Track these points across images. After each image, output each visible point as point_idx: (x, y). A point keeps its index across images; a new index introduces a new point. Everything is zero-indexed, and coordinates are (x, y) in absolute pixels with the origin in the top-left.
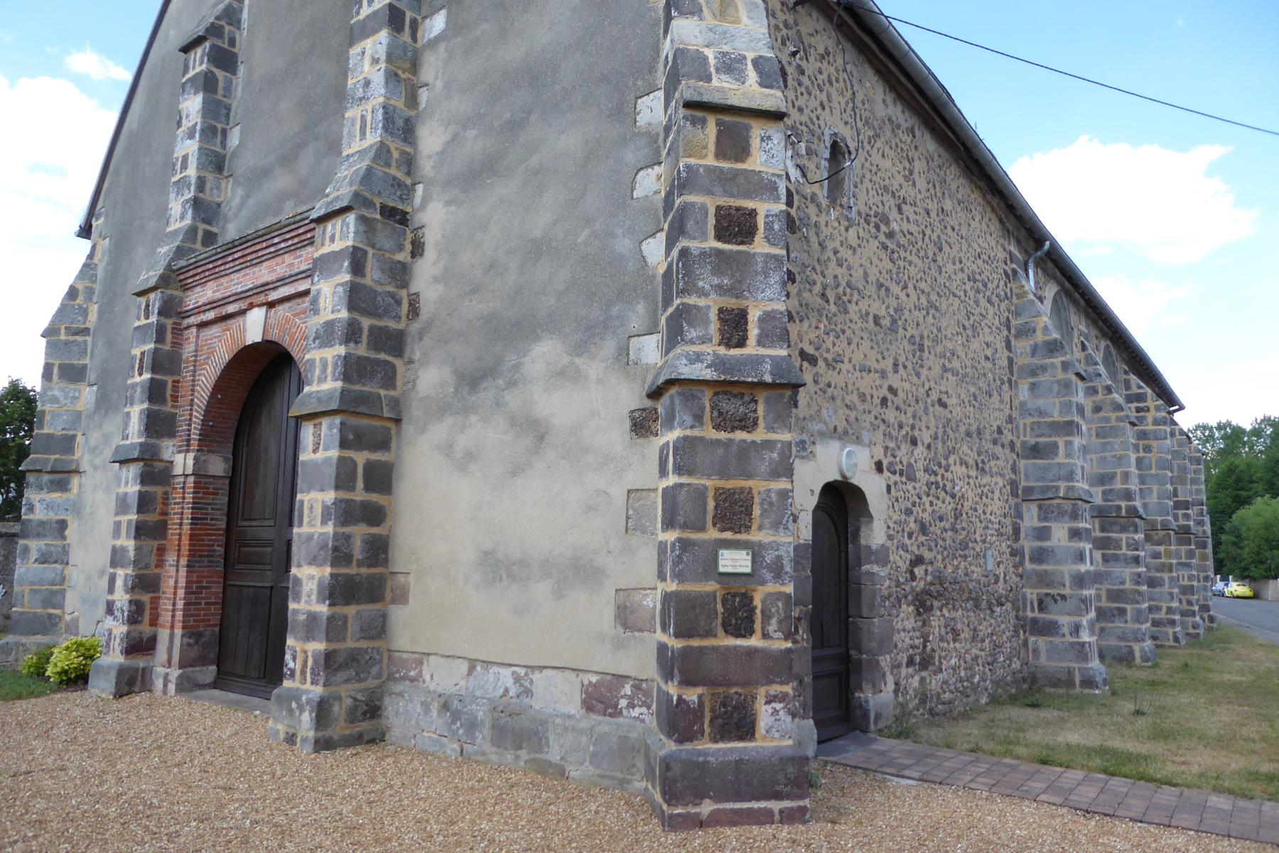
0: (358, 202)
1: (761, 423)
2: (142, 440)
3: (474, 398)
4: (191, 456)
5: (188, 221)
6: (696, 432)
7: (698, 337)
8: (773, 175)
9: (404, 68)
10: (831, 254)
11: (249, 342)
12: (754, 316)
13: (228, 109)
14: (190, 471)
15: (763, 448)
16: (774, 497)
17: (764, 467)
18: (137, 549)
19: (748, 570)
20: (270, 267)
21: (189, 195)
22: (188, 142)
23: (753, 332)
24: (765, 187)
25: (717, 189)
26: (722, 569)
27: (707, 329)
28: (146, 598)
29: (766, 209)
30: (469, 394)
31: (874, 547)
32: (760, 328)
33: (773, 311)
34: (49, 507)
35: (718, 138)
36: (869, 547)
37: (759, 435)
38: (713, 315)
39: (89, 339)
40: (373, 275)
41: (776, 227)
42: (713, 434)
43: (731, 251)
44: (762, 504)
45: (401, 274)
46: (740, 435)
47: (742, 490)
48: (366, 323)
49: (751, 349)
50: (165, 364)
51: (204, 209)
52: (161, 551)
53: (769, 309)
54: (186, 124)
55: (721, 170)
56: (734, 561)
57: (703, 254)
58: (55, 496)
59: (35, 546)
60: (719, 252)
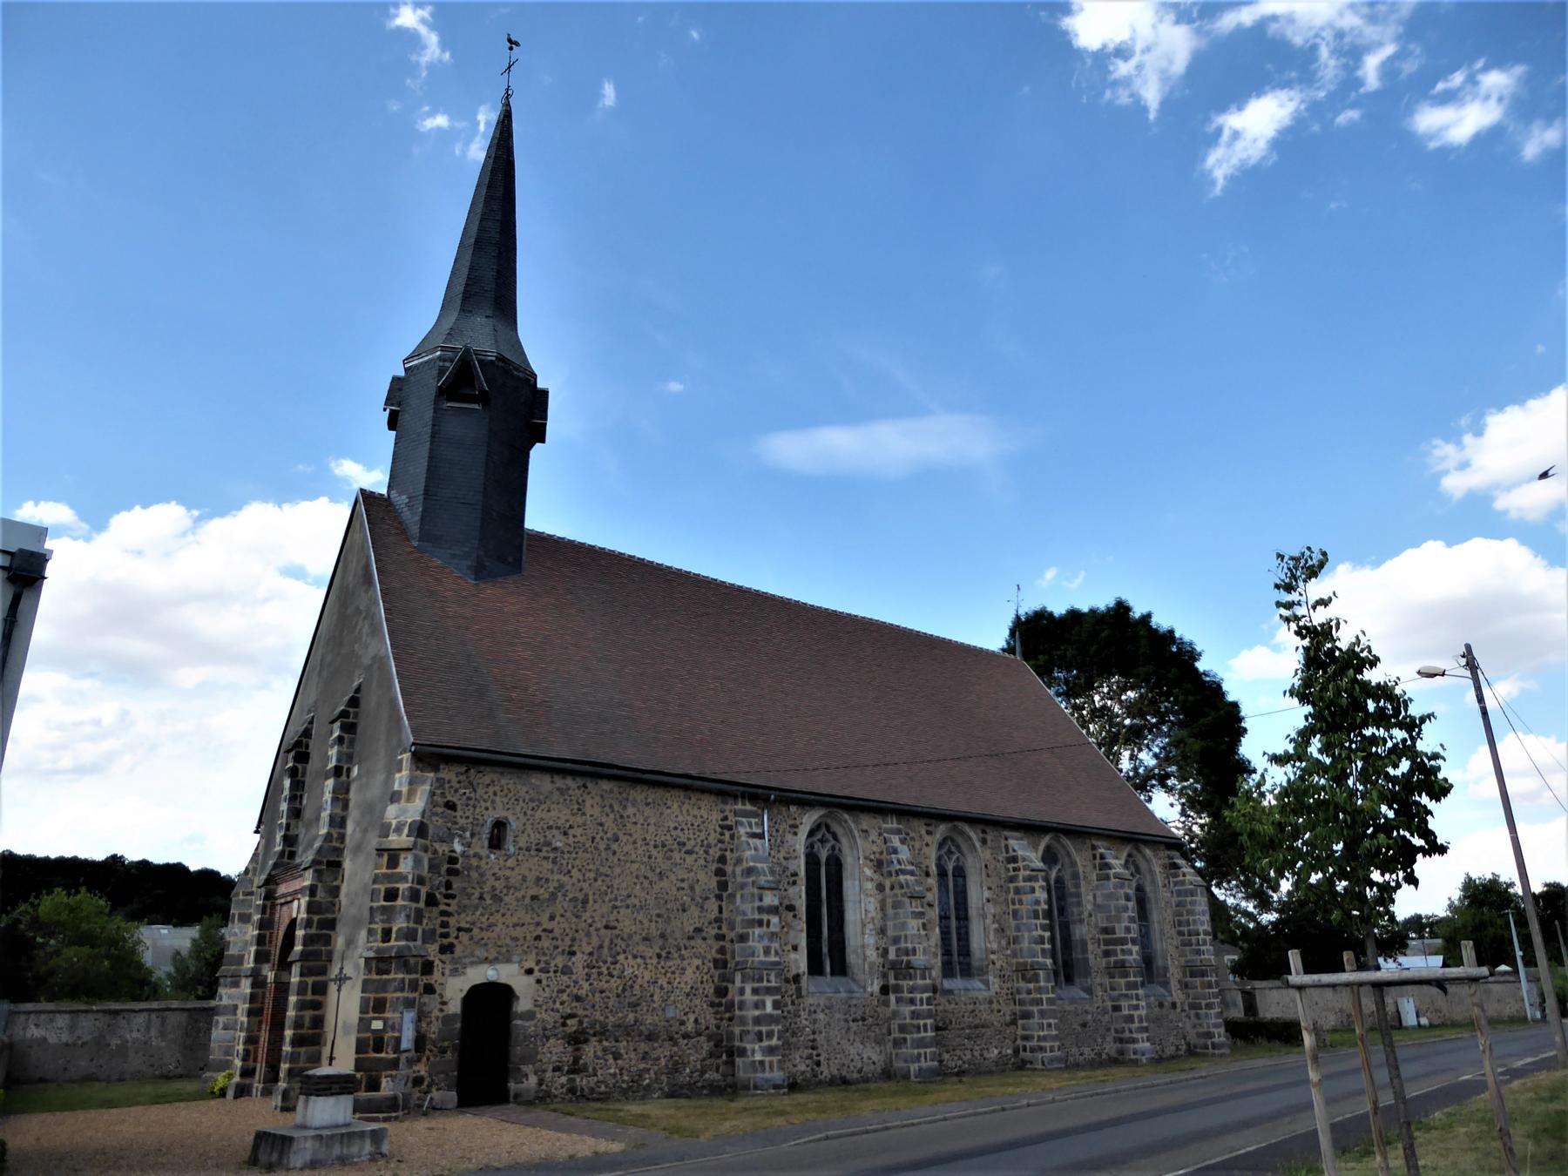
0: (315, 862)
9: (341, 797)
24: (403, 878)
28: (251, 1048)
29: (403, 887)
34: (230, 997)
37: (392, 976)
40: (321, 895)
42: (375, 977)
45: (335, 892)
48: (316, 918)
49: (392, 943)
52: (260, 1022)
56: (377, 1025)
58: (233, 991)
59: (221, 1019)
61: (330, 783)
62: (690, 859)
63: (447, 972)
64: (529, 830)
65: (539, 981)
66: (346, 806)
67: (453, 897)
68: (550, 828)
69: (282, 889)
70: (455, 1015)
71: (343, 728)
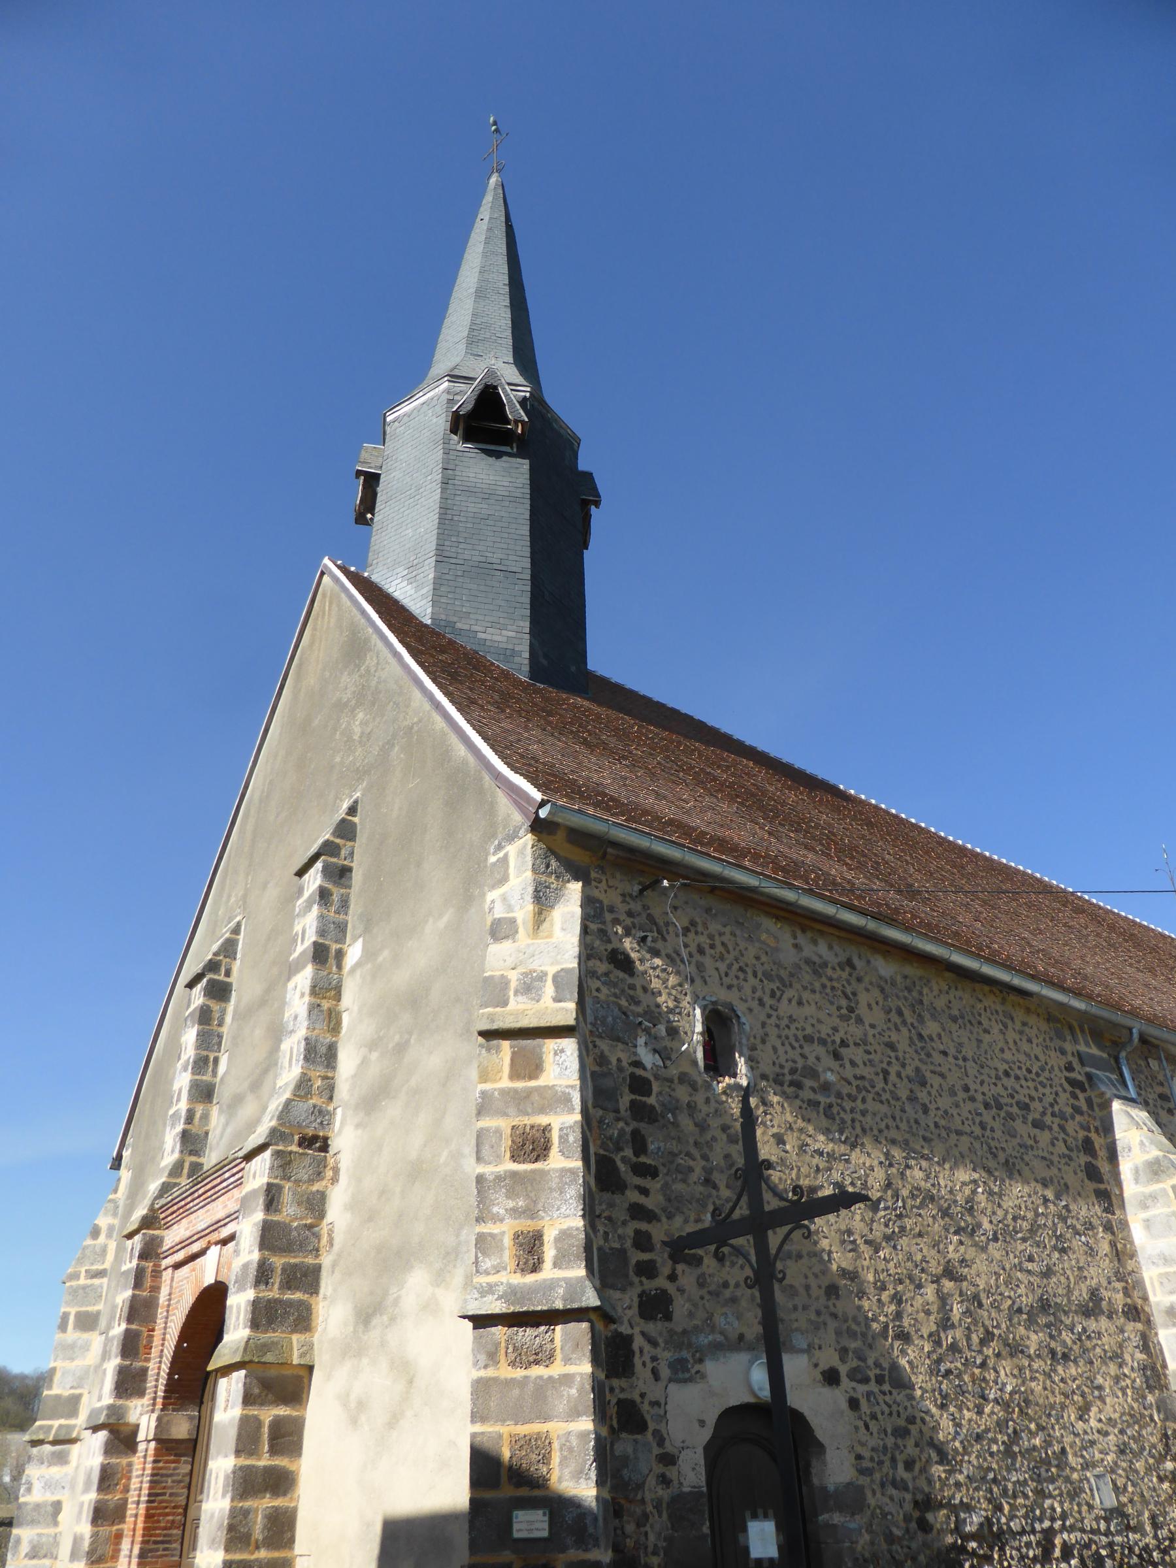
0: (275, 1135)
1: (559, 1355)
2: (111, 1401)
3: (366, 1338)
4: (154, 1416)
5: (176, 1155)
6: (490, 1373)
7: (493, 1267)
8: (567, 1087)
10: (718, 1133)
11: (206, 1284)
12: (550, 1236)
13: (220, 1037)
14: (151, 1437)
15: (561, 1384)
16: (574, 1442)
17: (561, 1406)
18: (95, 1536)
19: (545, 1534)
20: (224, 1202)
21: (180, 1127)
22: (184, 1074)
23: (549, 1252)
25: (512, 1111)
26: (516, 1535)
27: (501, 1257)
30: (364, 1332)
31: (831, 1488)
32: (556, 1248)
33: (570, 1228)
34: (48, 1485)
35: (512, 1060)
36: (824, 1489)
37: (557, 1369)
38: (507, 1241)
39: (105, 1280)
41: (571, 1139)
43: (525, 1171)
44: (561, 1449)
45: (316, 1205)
46: (537, 1371)
47: (538, 1436)
48: (278, 1261)
49: (548, 1272)
50: (141, 1311)
51: (192, 1142)
52: (119, 1536)
53: (565, 1226)
54: (184, 1057)
55: (515, 1091)
57: (499, 1178)
58: (55, 1471)
60: (514, 1174)
61: (305, 977)
62: (1044, 1137)
63: (665, 1372)
64: (773, 1040)
65: (854, 1404)
66: (334, 1025)
67: (652, 1172)
68: (809, 1039)
69: (171, 1237)
70: (695, 1495)
71: (327, 872)
